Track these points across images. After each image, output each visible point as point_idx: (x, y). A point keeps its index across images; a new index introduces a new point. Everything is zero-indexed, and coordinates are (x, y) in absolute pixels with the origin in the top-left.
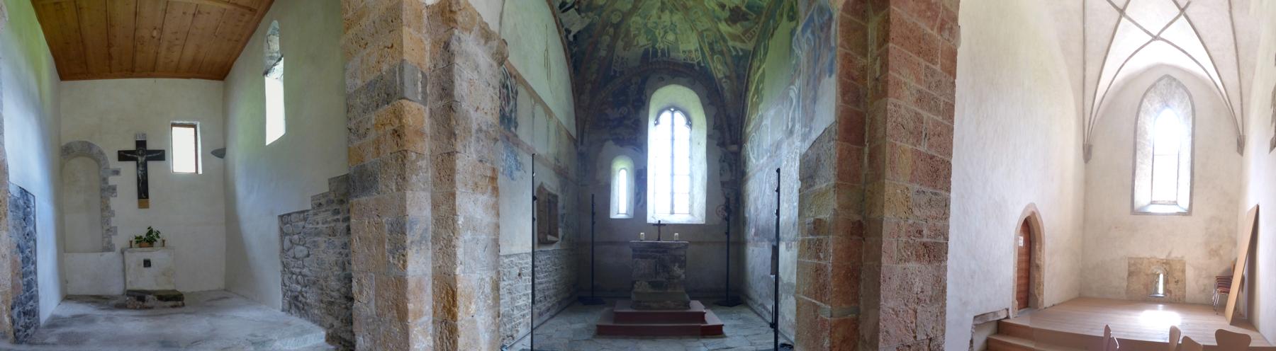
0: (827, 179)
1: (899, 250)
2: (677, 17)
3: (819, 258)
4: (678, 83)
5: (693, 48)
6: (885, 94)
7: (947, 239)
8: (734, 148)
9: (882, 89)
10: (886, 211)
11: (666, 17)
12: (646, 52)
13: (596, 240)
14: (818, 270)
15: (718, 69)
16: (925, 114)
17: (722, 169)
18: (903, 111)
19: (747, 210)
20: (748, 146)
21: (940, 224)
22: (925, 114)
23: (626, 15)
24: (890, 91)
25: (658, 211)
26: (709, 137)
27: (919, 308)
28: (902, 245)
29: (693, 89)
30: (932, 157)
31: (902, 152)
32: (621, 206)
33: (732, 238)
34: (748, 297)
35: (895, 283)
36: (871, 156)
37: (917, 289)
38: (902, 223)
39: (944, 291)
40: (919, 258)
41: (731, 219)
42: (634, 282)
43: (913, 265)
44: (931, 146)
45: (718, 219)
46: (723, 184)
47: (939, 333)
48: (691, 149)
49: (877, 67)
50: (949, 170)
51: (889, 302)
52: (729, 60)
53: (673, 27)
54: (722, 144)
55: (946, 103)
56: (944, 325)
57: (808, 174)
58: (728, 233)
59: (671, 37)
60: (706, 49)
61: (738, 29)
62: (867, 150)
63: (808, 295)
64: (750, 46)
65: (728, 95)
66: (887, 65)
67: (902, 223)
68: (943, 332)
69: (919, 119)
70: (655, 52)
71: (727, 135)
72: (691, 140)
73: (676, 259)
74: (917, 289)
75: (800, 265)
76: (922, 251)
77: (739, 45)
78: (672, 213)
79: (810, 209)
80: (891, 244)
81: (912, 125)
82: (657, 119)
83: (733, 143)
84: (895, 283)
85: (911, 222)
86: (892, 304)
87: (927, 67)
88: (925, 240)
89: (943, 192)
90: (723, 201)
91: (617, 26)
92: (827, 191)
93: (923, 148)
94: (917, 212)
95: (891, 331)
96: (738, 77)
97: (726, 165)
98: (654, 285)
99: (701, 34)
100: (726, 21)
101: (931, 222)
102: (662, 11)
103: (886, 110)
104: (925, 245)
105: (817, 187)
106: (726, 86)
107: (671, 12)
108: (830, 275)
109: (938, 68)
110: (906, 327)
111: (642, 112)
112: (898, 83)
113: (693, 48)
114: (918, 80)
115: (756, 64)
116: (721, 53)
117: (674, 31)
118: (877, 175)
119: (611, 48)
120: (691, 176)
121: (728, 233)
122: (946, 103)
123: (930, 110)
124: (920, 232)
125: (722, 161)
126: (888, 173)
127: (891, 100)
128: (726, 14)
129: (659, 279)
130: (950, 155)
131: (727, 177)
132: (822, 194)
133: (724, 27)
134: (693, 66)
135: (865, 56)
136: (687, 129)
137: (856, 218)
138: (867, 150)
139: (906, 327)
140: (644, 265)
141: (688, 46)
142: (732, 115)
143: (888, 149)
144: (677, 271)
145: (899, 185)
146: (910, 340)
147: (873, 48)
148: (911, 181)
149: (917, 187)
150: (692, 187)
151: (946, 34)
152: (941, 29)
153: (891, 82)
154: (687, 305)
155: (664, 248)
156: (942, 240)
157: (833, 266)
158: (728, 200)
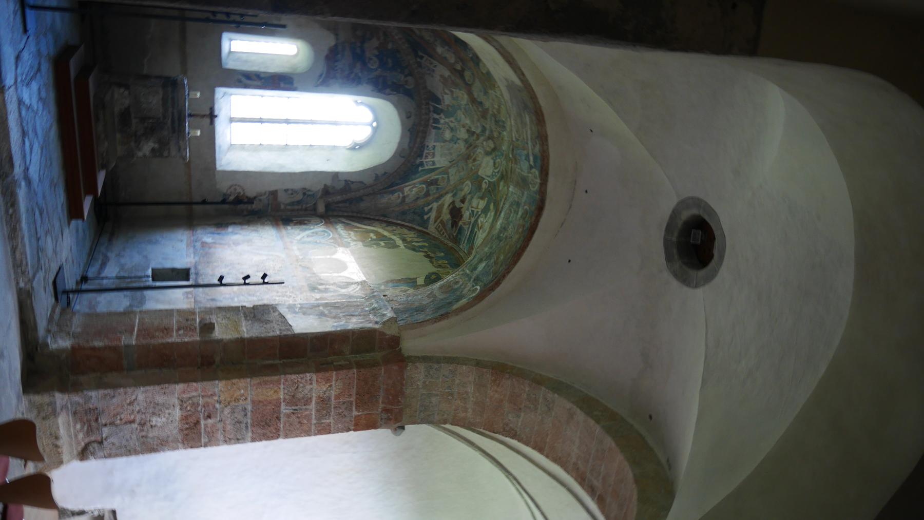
0: (248, 330)
1: (190, 398)
2: (461, 146)
3: (179, 329)
4: (403, 137)
5: (435, 159)
6: (318, 371)
7: (206, 446)
8: (321, 208)
9: (321, 367)
10: (224, 382)
11: (462, 134)
12: (438, 100)
13: (190, 24)
14: (167, 330)
15: (412, 189)
16: (313, 406)
17: (294, 192)
18: (308, 387)
19: (237, 229)
20: (320, 228)
21: (220, 436)
22: (313, 406)
23: (468, 87)
24: (321, 375)
25: (233, 104)
26: (336, 175)
27: (135, 426)
28: (195, 400)
29: (394, 156)
30: (278, 418)
31: (278, 389)
32: (241, 47)
33: (197, 208)
34: (112, 236)
35: (160, 399)
36: (271, 366)
37: (155, 420)
38: (216, 398)
39: (153, 450)
40: (185, 418)
41: (226, 207)
42: (127, 87)
43: (177, 413)
44: (288, 416)
45: (224, 186)
46: (274, 194)
47: (106, 452)
48: (322, 148)
49: (343, 363)
50: (272, 438)
51: (141, 395)
52: (421, 202)
53: (454, 140)
54: (326, 192)
55: (329, 425)
56: (116, 455)
57: (258, 313)
58: (204, 202)
59: (448, 135)
60: (433, 176)
61: (446, 216)
62: (277, 362)
63: (141, 322)
64: (432, 228)
65: (384, 200)
66: (339, 369)
67: (216, 398)
68: (109, 456)
69: (308, 401)
70: (438, 111)
71: (339, 198)
72: (334, 147)
73: (163, 144)
74: (155, 420)
75: (169, 313)
76: (192, 420)
77: (433, 215)
78: (232, 120)
79: (225, 317)
80: (196, 390)
81: (300, 396)
82: (362, 103)
83: (328, 206)
84: (160, 399)
85: (217, 406)
86: (141, 397)
87: (351, 403)
88: (202, 422)
89: (250, 434)
90: (251, 193)
91: (461, 73)
92: (238, 332)
93: (284, 409)
94: (227, 411)
95: (115, 400)
96: (404, 213)
97: (299, 197)
98: (125, 116)
99: (445, 171)
100: (453, 203)
101: (220, 426)
102: (468, 131)
103: (305, 372)
104: (197, 423)
105: (244, 322)
106: (395, 197)
107: (466, 141)
108: (164, 341)
109: (355, 413)
110: (115, 415)
111: (369, 88)
112: (328, 380)
113: (435, 159)
114: (337, 397)
115: (410, 235)
116: (427, 194)
117: (451, 140)
118: (253, 371)
119: (443, 61)
120: (286, 147)
121: (204, 202)
122: (329, 425)
123: (318, 411)
124: (209, 417)
125: (305, 192)
126: (256, 381)
127: (314, 377)
128: (458, 205)
129: (134, 121)
130: (286, 436)
131: (283, 198)
132: (237, 327)
133: (448, 199)
134: (421, 156)
135: (352, 353)
136: (348, 143)
137: (217, 359)
138: (277, 362)
139: (115, 415)
140: (153, 101)
141: (439, 156)
142: (363, 205)
143: (275, 378)
144: (148, 147)
145: (247, 391)
146: (103, 420)
147: (359, 357)
148: (253, 402)
149: (249, 408)
150: (270, 148)
151: (385, 416)
152: (386, 410)
153: (327, 374)
154: (103, 167)
155: (179, 122)
156: (204, 440)
157: (173, 344)
158: (251, 201)
